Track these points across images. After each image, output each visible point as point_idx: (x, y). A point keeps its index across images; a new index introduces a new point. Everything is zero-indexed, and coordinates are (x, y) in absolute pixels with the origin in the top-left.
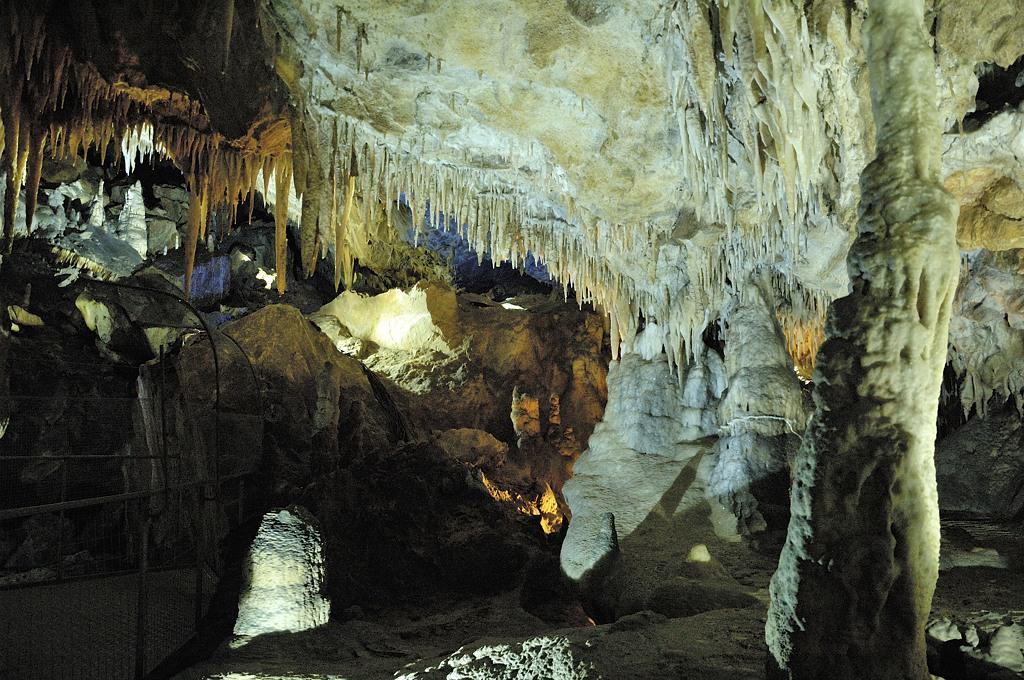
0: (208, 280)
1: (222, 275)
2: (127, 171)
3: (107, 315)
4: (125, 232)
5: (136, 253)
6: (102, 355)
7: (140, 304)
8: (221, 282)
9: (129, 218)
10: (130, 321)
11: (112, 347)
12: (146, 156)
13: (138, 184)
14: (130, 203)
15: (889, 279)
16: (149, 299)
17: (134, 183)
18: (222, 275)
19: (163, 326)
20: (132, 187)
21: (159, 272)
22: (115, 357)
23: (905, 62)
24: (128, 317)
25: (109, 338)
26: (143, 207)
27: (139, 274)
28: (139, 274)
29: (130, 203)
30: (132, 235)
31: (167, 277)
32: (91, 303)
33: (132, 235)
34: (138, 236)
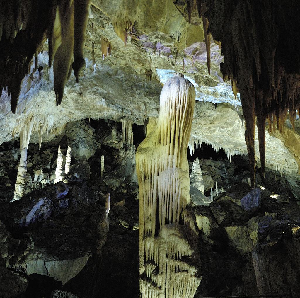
0: (252, 200)
1: (258, 197)
2: (191, 154)
3: (208, 222)
4: (194, 182)
5: (200, 192)
6: (204, 242)
7: (222, 215)
8: (257, 201)
9: (195, 176)
10: (218, 224)
11: (210, 237)
12: (199, 146)
13: (197, 159)
14: (195, 169)
15: (191, 168)
16: (226, 212)
17: (196, 159)
18: (258, 197)
19: (234, 225)
20: (195, 161)
21: (229, 198)
22: (212, 242)
23: (126, 117)
24: (217, 222)
25: (209, 233)
26: (200, 170)
27: (218, 201)
28: (218, 201)
29: (195, 169)
30: (197, 184)
31: (234, 201)
32: (200, 216)
33: (197, 184)
34: (200, 184)
